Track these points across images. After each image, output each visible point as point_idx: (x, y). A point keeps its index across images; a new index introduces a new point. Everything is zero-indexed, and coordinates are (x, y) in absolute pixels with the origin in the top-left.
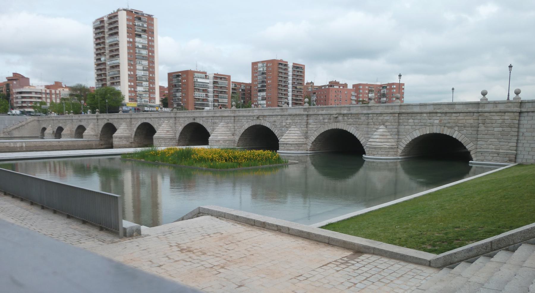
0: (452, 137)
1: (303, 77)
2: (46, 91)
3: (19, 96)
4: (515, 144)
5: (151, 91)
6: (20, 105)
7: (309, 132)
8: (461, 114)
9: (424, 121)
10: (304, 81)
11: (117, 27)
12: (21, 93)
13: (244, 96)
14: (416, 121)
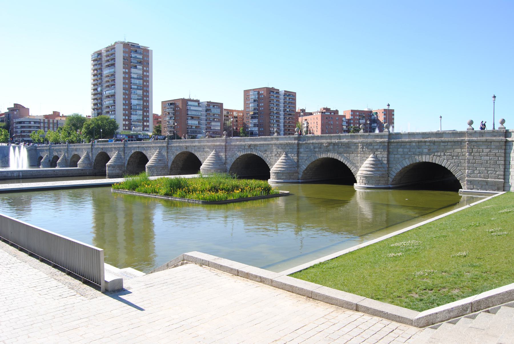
0: (441, 165)
1: (295, 104)
2: (44, 120)
3: (19, 126)
4: (502, 173)
5: (145, 119)
6: (19, 134)
7: (300, 161)
8: (449, 144)
9: (414, 150)
10: (295, 107)
11: (114, 59)
12: (20, 123)
13: (233, 127)
14: (406, 150)
